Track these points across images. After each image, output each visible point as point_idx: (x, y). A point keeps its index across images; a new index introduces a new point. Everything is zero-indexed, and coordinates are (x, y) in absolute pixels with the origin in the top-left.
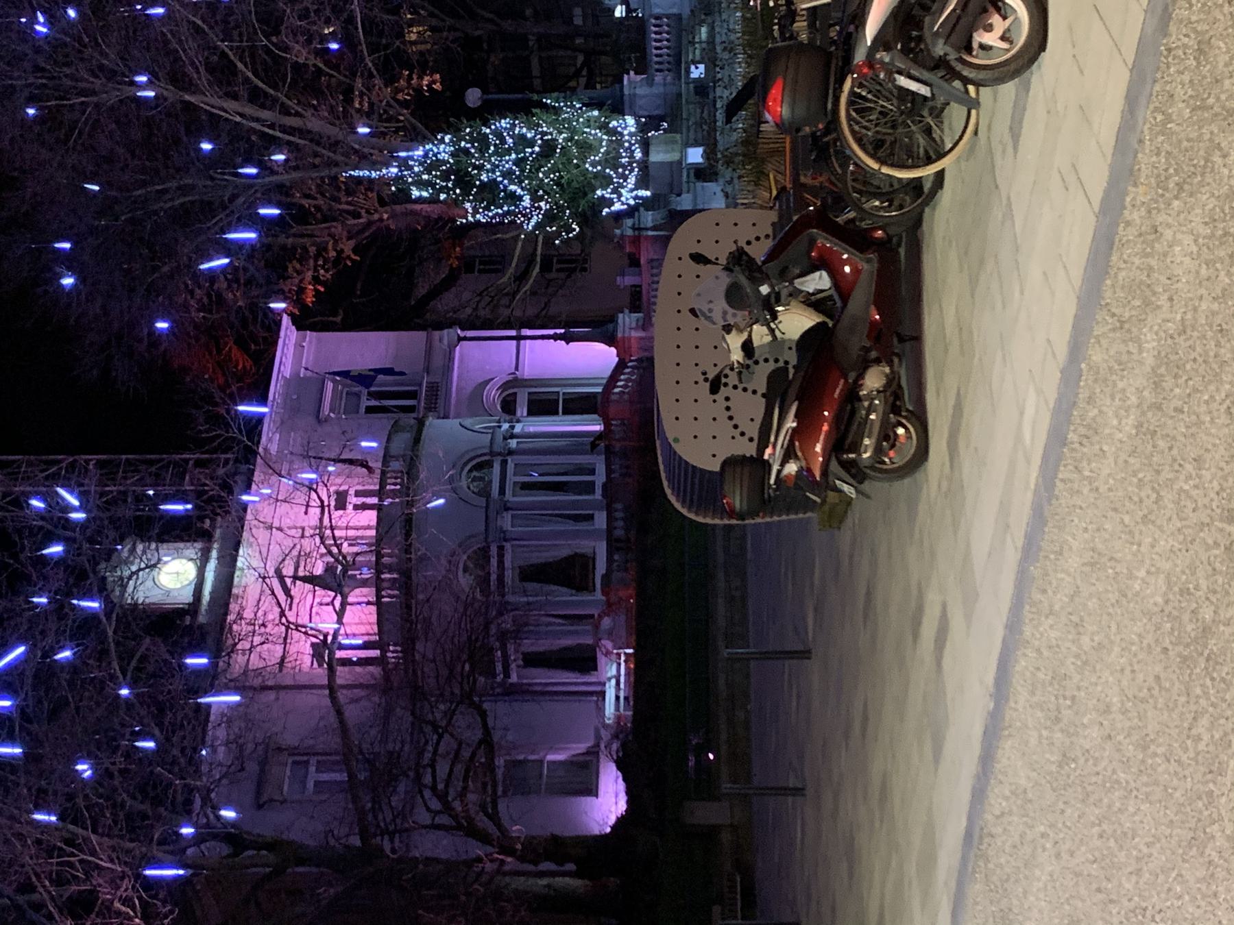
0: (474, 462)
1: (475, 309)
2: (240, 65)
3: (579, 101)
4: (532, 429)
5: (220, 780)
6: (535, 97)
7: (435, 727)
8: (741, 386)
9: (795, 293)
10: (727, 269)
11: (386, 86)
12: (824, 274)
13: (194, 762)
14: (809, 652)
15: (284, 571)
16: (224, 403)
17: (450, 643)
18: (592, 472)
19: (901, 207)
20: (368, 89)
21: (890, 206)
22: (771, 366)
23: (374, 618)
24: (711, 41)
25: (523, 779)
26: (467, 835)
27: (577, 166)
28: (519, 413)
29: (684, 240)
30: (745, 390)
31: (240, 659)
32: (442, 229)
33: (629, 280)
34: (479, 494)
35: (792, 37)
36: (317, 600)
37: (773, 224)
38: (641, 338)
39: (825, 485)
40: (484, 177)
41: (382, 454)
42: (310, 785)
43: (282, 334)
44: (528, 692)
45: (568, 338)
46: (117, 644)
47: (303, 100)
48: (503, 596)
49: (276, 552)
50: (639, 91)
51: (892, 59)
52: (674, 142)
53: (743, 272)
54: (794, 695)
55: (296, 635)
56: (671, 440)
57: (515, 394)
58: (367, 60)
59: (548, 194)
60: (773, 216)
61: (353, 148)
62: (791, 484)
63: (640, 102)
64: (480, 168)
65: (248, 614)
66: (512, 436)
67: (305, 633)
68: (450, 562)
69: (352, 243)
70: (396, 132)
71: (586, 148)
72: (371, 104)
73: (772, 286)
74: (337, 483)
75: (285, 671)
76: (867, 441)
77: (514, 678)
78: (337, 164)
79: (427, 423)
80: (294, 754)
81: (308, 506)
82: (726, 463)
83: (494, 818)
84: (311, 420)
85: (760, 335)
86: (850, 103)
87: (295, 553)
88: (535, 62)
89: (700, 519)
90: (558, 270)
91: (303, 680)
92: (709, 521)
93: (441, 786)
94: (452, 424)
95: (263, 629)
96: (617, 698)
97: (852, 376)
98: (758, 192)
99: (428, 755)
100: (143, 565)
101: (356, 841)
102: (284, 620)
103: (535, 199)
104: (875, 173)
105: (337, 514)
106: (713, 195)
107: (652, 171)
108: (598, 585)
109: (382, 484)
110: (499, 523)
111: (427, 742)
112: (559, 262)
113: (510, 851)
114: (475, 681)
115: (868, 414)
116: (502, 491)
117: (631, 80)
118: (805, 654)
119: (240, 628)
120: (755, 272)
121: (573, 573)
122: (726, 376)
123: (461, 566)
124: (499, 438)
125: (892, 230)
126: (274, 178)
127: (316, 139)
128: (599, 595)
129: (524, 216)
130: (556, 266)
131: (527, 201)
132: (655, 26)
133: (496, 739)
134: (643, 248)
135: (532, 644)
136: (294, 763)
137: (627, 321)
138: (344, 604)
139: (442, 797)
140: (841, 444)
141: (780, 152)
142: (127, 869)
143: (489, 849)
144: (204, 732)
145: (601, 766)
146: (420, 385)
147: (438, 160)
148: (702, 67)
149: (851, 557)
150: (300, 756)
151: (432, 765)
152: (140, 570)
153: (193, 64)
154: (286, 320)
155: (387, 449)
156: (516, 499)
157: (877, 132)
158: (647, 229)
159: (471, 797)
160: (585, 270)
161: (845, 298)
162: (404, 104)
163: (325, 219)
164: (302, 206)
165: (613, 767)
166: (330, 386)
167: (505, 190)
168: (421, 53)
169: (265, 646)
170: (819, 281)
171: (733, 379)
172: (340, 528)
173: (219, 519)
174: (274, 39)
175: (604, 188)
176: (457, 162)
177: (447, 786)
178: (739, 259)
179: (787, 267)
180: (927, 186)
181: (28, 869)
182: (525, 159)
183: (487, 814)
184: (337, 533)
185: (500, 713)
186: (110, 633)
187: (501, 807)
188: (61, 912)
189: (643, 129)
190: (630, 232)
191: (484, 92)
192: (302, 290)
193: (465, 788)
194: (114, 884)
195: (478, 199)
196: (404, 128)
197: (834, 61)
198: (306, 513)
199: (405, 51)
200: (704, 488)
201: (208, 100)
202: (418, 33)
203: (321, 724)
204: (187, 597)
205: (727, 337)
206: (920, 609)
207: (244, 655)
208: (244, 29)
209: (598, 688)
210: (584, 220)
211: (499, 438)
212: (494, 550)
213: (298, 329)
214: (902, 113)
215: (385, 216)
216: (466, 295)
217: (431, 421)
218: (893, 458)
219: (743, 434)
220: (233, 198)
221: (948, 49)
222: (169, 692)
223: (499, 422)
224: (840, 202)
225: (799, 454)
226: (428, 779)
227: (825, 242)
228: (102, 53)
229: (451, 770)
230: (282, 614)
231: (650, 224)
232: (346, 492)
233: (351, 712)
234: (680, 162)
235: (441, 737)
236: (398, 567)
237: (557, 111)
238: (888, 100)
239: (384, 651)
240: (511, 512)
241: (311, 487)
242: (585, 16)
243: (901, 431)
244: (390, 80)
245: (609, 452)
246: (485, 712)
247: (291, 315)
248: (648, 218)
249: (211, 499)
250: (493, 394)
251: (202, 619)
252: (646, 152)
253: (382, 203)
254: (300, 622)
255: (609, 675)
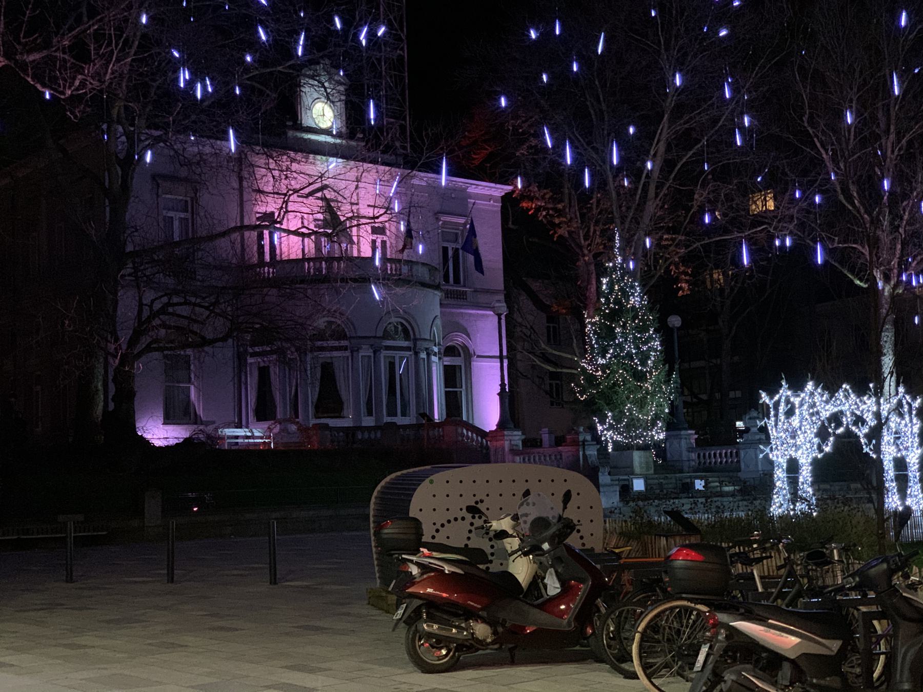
0: (409, 328)
1: (521, 325)
2: (691, 153)
3: (675, 398)
4: (434, 368)
5: (174, 149)
6: (677, 366)
7: (217, 303)
8: (473, 528)
9: (543, 568)
10: (560, 518)
11: (679, 258)
12: (559, 590)
13: (186, 130)
14: (275, 583)
15: (328, 193)
16: (448, 147)
17: (278, 314)
18: (404, 414)
19: (609, 646)
20: (677, 246)
21: (610, 638)
22: (488, 551)
23: (293, 257)
24: (722, 494)
25: (177, 369)
26: (135, 331)
27: (628, 398)
28: (446, 359)
29: (578, 482)
30: (470, 531)
31: (261, 160)
32: (579, 302)
33: (546, 438)
34: (385, 330)
35: (732, 562)
36: (305, 216)
37: (592, 549)
38: (503, 448)
39: (402, 596)
40: (618, 330)
41: (414, 260)
42: (171, 214)
43: (498, 186)
44: (240, 372)
45: (501, 394)
46: (271, 73)
47: (668, 198)
48: (311, 351)
49: (341, 185)
50: (683, 442)
51: (721, 641)
52: (648, 469)
53: (559, 530)
54: (243, 572)
55: (280, 201)
56: (431, 477)
57: (460, 356)
58: (698, 244)
59: (607, 378)
60: (599, 549)
61: (635, 234)
62: (402, 568)
63: (675, 442)
64: (624, 327)
65: (295, 166)
66: (428, 355)
67: (282, 208)
68: (335, 311)
69: (566, 235)
70: (647, 265)
71: (641, 404)
72: (666, 247)
73: (548, 551)
74: (390, 228)
75: (254, 194)
76: (435, 626)
77: (250, 360)
78: (622, 223)
79: (436, 292)
80: (192, 201)
81: (374, 207)
82: (416, 520)
83: (148, 349)
84: (438, 208)
85: (512, 544)
86: (686, 609)
87: (340, 198)
88: (702, 363)
89: (373, 500)
90: (551, 385)
91: (247, 207)
92: (372, 506)
93: (170, 310)
94: (437, 310)
95: (283, 177)
96: (237, 437)
97: (483, 614)
98: (616, 536)
99: (193, 300)
100: (329, 90)
101: (129, 248)
102: (291, 192)
103: (604, 367)
104: (634, 627)
105: (369, 228)
106: (610, 499)
107: (626, 453)
108: (323, 421)
109: (391, 260)
110: (364, 347)
111: (204, 298)
112: (557, 384)
113: (122, 363)
114: (249, 332)
115: (456, 627)
116: (388, 348)
117: (691, 435)
118: (274, 581)
119: (285, 162)
120: (558, 539)
121: (330, 402)
122: (480, 518)
123: (333, 320)
124: (425, 345)
125: (592, 641)
126: (611, 179)
127: (641, 207)
128: (313, 421)
129: (591, 359)
130: (554, 382)
131: (601, 361)
132: (731, 453)
133: (206, 349)
134: (570, 448)
135: (275, 373)
136: (186, 201)
137: (516, 437)
138: (303, 235)
139: (163, 311)
140: (433, 607)
141: (645, 554)
142: (107, 84)
143: (124, 347)
144: (209, 137)
145: (186, 426)
146: (464, 286)
147: (629, 296)
148: (701, 488)
149: (349, 614)
150: (191, 206)
151: (186, 303)
152: (325, 88)
153: (691, 118)
154: (510, 188)
155: (417, 263)
156: (382, 360)
157: (664, 629)
158: (584, 451)
159: (163, 332)
160: (552, 404)
161: (541, 607)
162: (667, 271)
163: (583, 216)
164: (591, 198)
165: (186, 435)
166: (462, 221)
167: (609, 345)
168: (704, 282)
169: (271, 179)
170: (553, 586)
171: (478, 522)
172: (358, 231)
173: (363, 144)
174: (710, 177)
175: (613, 418)
176: (628, 310)
177: (170, 314)
178: (568, 527)
179: (562, 562)
180: (625, 666)
181: (106, 12)
182: (632, 359)
183: (150, 343)
184: (355, 229)
185: (227, 351)
186: (280, 68)
187: (156, 355)
188: (75, 37)
189: (657, 445)
190: (581, 438)
191: (678, 329)
192: (531, 199)
193: (170, 327)
194: (98, 76)
195: (602, 326)
196: (650, 270)
197: (719, 598)
198: (369, 206)
199: (706, 270)
200: (397, 504)
201: (664, 131)
202: (719, 280)
203: (216, 222)
204: (307, 122)
205: (509, 518)
206: (312, 671)
207: (266, 164)
208: (716, 155)
209: (244, 423)
210: (590, 402)
211: (425, 345)
212: (344, 343)
213: (502, 197)
214: (680, 648)
215: (587, 258)
216: (530, 318)
217: (438, 295)
218: (423, 646)
219: (437, 531)
220: (595, 149)
221: (729, 683)
222: (237, 112)
223: (439, 344)
224: (611, 600)
225: (425, 576)
226: (175, 300)
227: (583, 589)
228: (695, 56)
229: (183, 317)
230: (296, 191)
231: (588, 453)
232: (385, 235)
233: (223, 242)
234: (633, 474)
235: (207, 308)
236: (330, 271)
237: (667, 382)
238: (689, 638)
239: (269, 265)
240: (372, 355)
241: (388, 209)
242: (735, 399)
243: (444, 652)
244: (684, 260)
245: (417, 427)
246: (226, 340)
247: (513, 192)
248: (592, 452)
249: (376, 137)
250: (460, 339)
251: (291, 133)
252: (639, 448)
253: (596, 256)
254: (290, 204)
255: (254, 430)
